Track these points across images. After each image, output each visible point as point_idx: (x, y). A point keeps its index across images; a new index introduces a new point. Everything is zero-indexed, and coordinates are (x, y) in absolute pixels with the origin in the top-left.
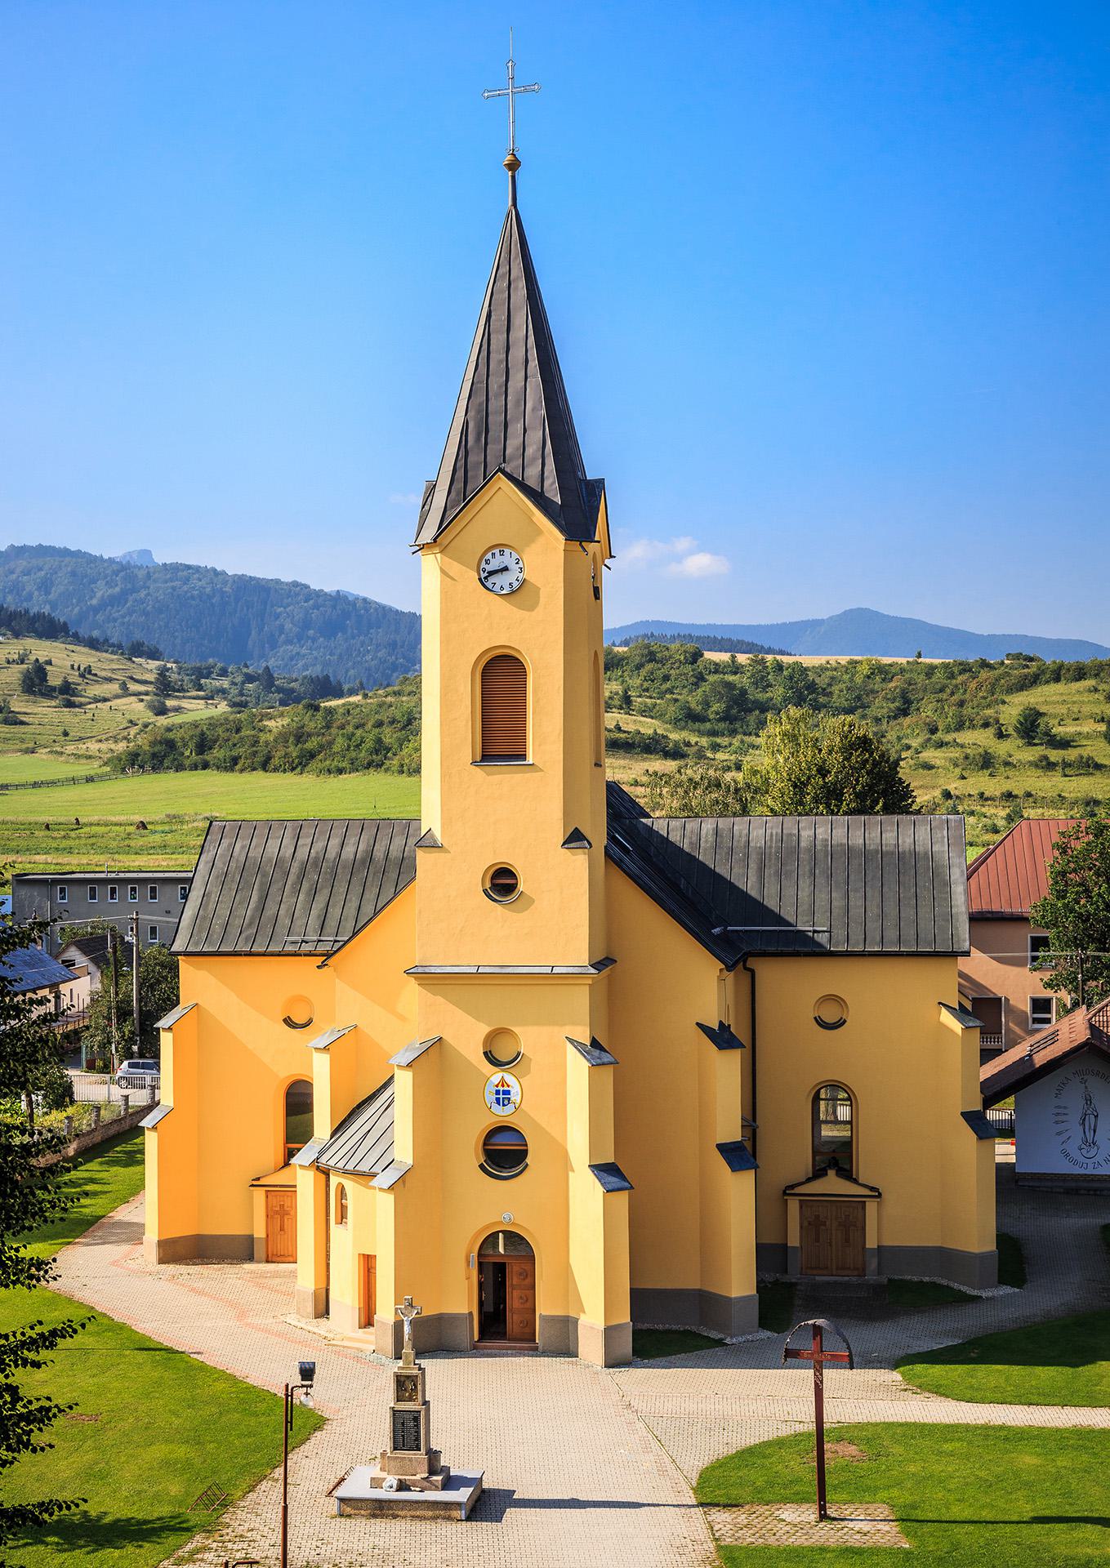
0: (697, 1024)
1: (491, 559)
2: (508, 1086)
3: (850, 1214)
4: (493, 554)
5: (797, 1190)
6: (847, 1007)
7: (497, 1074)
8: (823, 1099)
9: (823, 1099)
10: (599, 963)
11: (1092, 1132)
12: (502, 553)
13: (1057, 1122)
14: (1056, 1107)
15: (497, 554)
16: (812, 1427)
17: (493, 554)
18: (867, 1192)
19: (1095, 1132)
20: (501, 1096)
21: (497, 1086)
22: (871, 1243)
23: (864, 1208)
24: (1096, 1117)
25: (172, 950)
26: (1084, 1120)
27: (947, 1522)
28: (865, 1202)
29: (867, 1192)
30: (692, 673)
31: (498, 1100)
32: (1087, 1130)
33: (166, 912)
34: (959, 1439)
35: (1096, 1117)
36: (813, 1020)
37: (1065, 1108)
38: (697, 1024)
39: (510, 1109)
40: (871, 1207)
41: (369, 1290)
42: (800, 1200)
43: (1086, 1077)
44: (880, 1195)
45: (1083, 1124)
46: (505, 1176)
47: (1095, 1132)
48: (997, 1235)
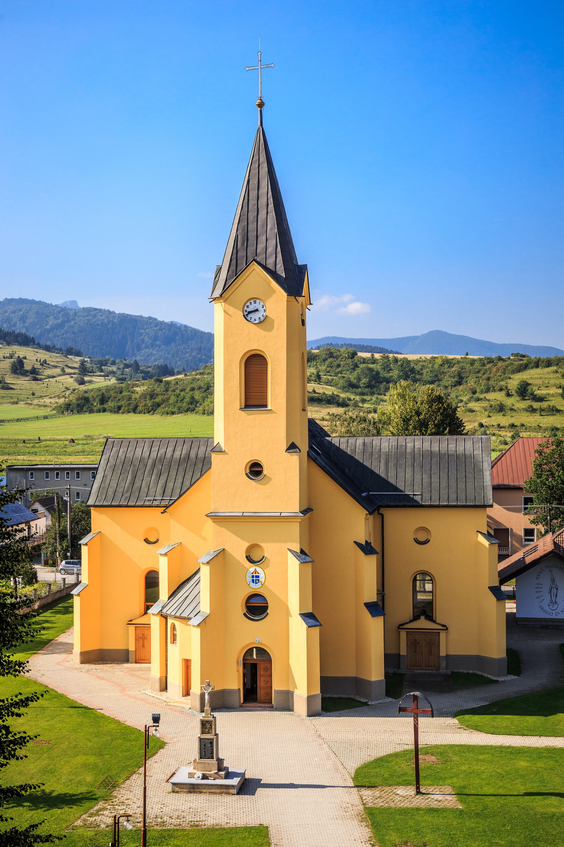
0: (355, 542)
2: (258, 573)
4: (251, 303)
5: (405, 626)
10: (304, 511)
11: (555, 597)
12: (255, 302)
13: (537, 592)
17: (251, 303)
18: (440, 627)
19: (556, 596)
20: (255, 579)
21: (253, 573)
22: (443, 653)
24: (557, 589)
26: (551, 591)
27: (481, 795)
29: (440, 627)
31: (253, 580)
35: (557, 589)
37: (541, 584)
38: (355, 542)
39: (259, 585)
40: (443, 635)
43: (551, 569)
44: (447, 629)
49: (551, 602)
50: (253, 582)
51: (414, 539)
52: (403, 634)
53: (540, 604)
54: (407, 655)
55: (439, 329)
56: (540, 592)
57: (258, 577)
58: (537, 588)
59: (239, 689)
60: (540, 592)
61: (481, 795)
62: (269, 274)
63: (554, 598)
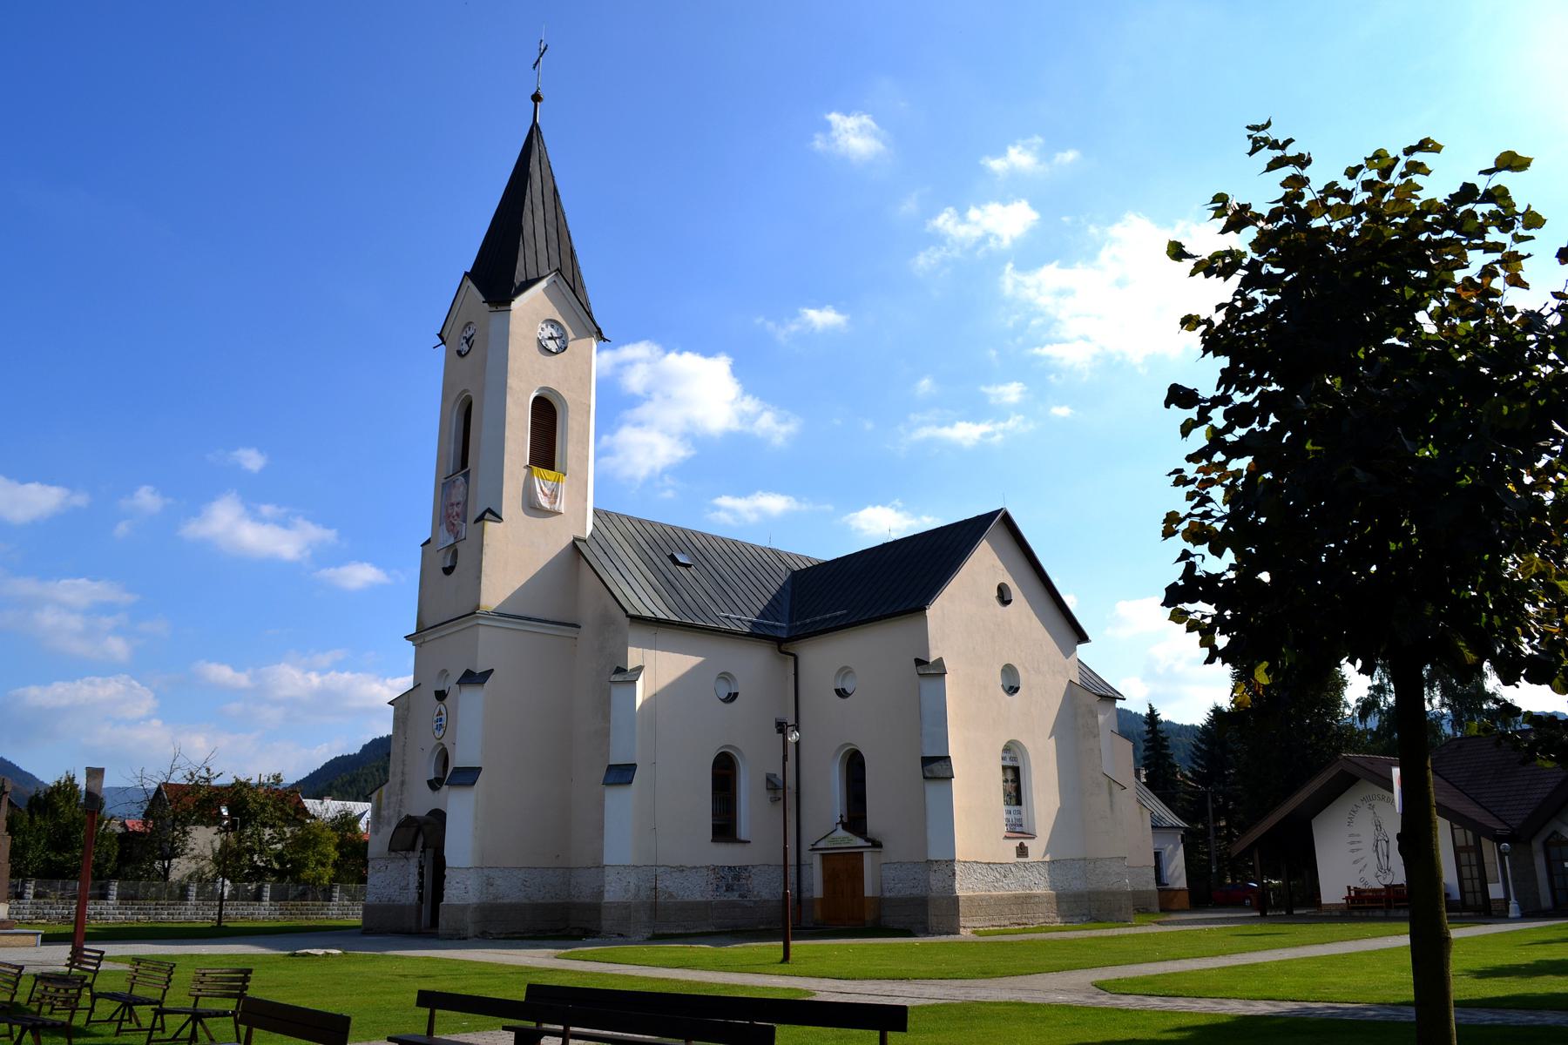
0: (491, 671)
5: (821, 845)
10: (607, 513)
11: (1386, 858)
13: (1353, 851)
14: (1350, 836)
16: (426, 627)
19: (1388, 858)
22: (868, 892)
24: (1387, 842)
26: (1377, 846)
27: (431, 628)
28: (862, 853)
32: (1380, 856)
33: (1013, 690)
34: (144, 914)
35: (1387, 842)
37: (1358, 835)
38: (491, 671)
40: (868, 859)
41: (529, 619)
42: (823, 854)
43: (1373, 803)
45: (1377, 851)
47: (1388, 858)
48: (713, 825)
49: (1380, 869)
53: (1362, 874)
56: (1358, 850)
58: (1352, 843)
59: (153, 1009)
60: (1358, 850)
61: (431, 628)
63: (1384, 861)
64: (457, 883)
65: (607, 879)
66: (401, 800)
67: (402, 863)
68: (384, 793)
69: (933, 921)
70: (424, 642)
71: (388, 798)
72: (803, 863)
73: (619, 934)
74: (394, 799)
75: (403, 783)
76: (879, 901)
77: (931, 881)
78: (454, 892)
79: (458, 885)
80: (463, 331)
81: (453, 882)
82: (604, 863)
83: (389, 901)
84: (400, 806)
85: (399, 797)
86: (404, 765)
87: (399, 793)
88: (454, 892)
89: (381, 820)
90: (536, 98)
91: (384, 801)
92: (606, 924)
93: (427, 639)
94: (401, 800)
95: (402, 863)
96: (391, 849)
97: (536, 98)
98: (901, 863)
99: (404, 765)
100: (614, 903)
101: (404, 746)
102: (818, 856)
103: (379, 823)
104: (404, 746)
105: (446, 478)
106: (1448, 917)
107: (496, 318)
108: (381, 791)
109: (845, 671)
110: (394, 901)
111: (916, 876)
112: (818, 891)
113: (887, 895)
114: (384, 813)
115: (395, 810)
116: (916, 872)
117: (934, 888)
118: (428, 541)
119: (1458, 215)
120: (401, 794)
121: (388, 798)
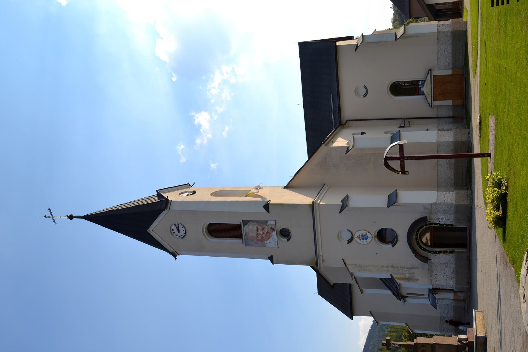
0: (340, 212)
1: (176, 234)
2: (360, 235)
3: (438, 81)
4: (174, 233)
5: (430, 102)
6: (355, 90)
7: (356, 239)
8: (477, 155)
9: (477, 155)
12: (173, 230)
15: (173, 232)
17: (174, 233)
18: (429, 75)
20: (364, 238)
21: (360, 239)
22: (449, 72)
23: (436, 76)
25: (404, 25)
28: (433, 76)
29: (429, 75)
30: (487, 30)
31: (365, 239)
36: (289, 241)
38: (340, 212)
39: (369, 235)
40: (436, 73)
42: (433, 101)
44: (430, 70)
46: (395, 243)
50: (367, 239)
51: (364, 97)
52: (436, 103)
54: (453, 100)
55: (383, 163)
57: (362, 236)
62: (471, 107)
64: (444, 197)
65: (443, 140)
66: (401, 268)
67: (434, 267)
68: (397, 276)
69: (462, 29)
70: (322, 256)
71: (399, 274)
72: (437, 116)
73: (468, 134)
74: (400, 271)
75: (392, 267)
76: (454, 68)
77: (446, 30)
78: (449, 199)
79: (445, 197)
80: (172, 234)
81: (444, 199)
82: (436, 141)
83: (453, 273)
84: (404, 268)
85: (400, 268)
86: (383, 266)
87: (397, 268)
88: (449, 199)
89: (411, 277)
90: (71, 217)
91: (401, 276)
92: (464, 139)
93: (321, 254)
94: (401, 268)
95: (434, 267)
96: (427, 262)
97: (71, 217)
98: (438, 58)
99: (383, 266)
100: (454, 137)
101: (374, 266)
102: (434, 102)
103: (412, 279)
104: (374, 266)
105: (243, 243)
106: (470, 153)
107: (173, 207)
108: (397, 278)
109: (356, 92)
110: (453, 270)
111: (443, 50)
112: (450, 102)
113: (451, 66)
114: (408, 276)
115: (406, 271)
116: (442, 50)
117: (448, 30)
118: (271, 259)
119: (197, 127)
120: (398, 267)
121: (399, 274)
